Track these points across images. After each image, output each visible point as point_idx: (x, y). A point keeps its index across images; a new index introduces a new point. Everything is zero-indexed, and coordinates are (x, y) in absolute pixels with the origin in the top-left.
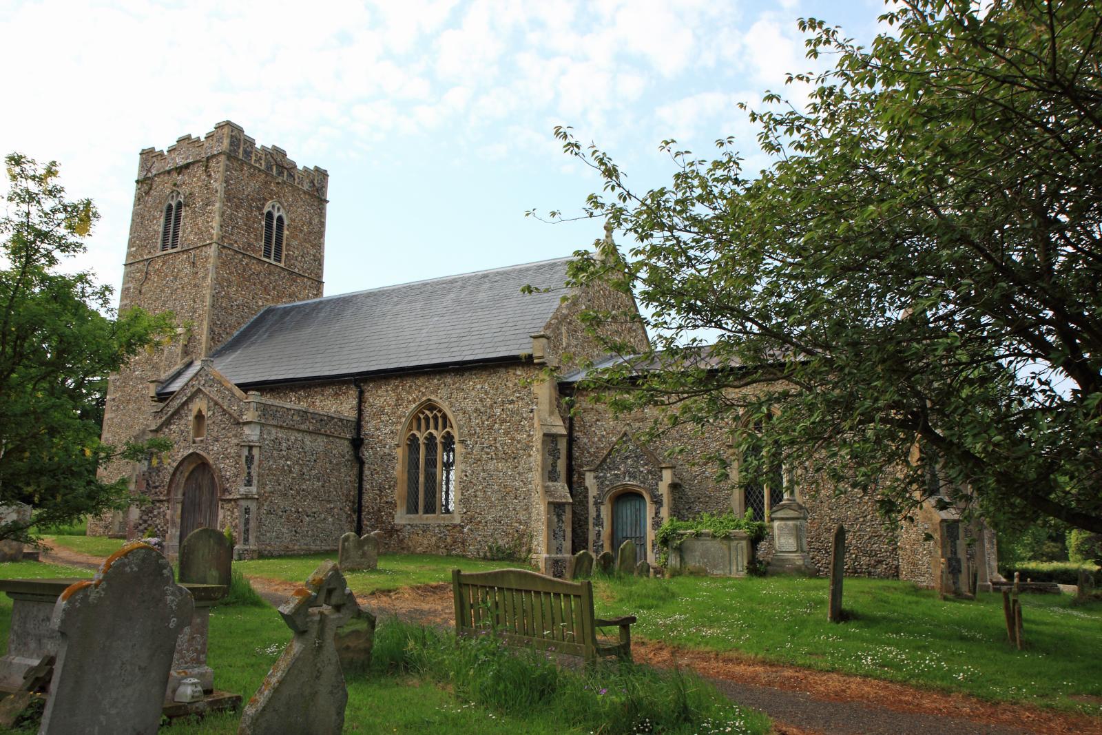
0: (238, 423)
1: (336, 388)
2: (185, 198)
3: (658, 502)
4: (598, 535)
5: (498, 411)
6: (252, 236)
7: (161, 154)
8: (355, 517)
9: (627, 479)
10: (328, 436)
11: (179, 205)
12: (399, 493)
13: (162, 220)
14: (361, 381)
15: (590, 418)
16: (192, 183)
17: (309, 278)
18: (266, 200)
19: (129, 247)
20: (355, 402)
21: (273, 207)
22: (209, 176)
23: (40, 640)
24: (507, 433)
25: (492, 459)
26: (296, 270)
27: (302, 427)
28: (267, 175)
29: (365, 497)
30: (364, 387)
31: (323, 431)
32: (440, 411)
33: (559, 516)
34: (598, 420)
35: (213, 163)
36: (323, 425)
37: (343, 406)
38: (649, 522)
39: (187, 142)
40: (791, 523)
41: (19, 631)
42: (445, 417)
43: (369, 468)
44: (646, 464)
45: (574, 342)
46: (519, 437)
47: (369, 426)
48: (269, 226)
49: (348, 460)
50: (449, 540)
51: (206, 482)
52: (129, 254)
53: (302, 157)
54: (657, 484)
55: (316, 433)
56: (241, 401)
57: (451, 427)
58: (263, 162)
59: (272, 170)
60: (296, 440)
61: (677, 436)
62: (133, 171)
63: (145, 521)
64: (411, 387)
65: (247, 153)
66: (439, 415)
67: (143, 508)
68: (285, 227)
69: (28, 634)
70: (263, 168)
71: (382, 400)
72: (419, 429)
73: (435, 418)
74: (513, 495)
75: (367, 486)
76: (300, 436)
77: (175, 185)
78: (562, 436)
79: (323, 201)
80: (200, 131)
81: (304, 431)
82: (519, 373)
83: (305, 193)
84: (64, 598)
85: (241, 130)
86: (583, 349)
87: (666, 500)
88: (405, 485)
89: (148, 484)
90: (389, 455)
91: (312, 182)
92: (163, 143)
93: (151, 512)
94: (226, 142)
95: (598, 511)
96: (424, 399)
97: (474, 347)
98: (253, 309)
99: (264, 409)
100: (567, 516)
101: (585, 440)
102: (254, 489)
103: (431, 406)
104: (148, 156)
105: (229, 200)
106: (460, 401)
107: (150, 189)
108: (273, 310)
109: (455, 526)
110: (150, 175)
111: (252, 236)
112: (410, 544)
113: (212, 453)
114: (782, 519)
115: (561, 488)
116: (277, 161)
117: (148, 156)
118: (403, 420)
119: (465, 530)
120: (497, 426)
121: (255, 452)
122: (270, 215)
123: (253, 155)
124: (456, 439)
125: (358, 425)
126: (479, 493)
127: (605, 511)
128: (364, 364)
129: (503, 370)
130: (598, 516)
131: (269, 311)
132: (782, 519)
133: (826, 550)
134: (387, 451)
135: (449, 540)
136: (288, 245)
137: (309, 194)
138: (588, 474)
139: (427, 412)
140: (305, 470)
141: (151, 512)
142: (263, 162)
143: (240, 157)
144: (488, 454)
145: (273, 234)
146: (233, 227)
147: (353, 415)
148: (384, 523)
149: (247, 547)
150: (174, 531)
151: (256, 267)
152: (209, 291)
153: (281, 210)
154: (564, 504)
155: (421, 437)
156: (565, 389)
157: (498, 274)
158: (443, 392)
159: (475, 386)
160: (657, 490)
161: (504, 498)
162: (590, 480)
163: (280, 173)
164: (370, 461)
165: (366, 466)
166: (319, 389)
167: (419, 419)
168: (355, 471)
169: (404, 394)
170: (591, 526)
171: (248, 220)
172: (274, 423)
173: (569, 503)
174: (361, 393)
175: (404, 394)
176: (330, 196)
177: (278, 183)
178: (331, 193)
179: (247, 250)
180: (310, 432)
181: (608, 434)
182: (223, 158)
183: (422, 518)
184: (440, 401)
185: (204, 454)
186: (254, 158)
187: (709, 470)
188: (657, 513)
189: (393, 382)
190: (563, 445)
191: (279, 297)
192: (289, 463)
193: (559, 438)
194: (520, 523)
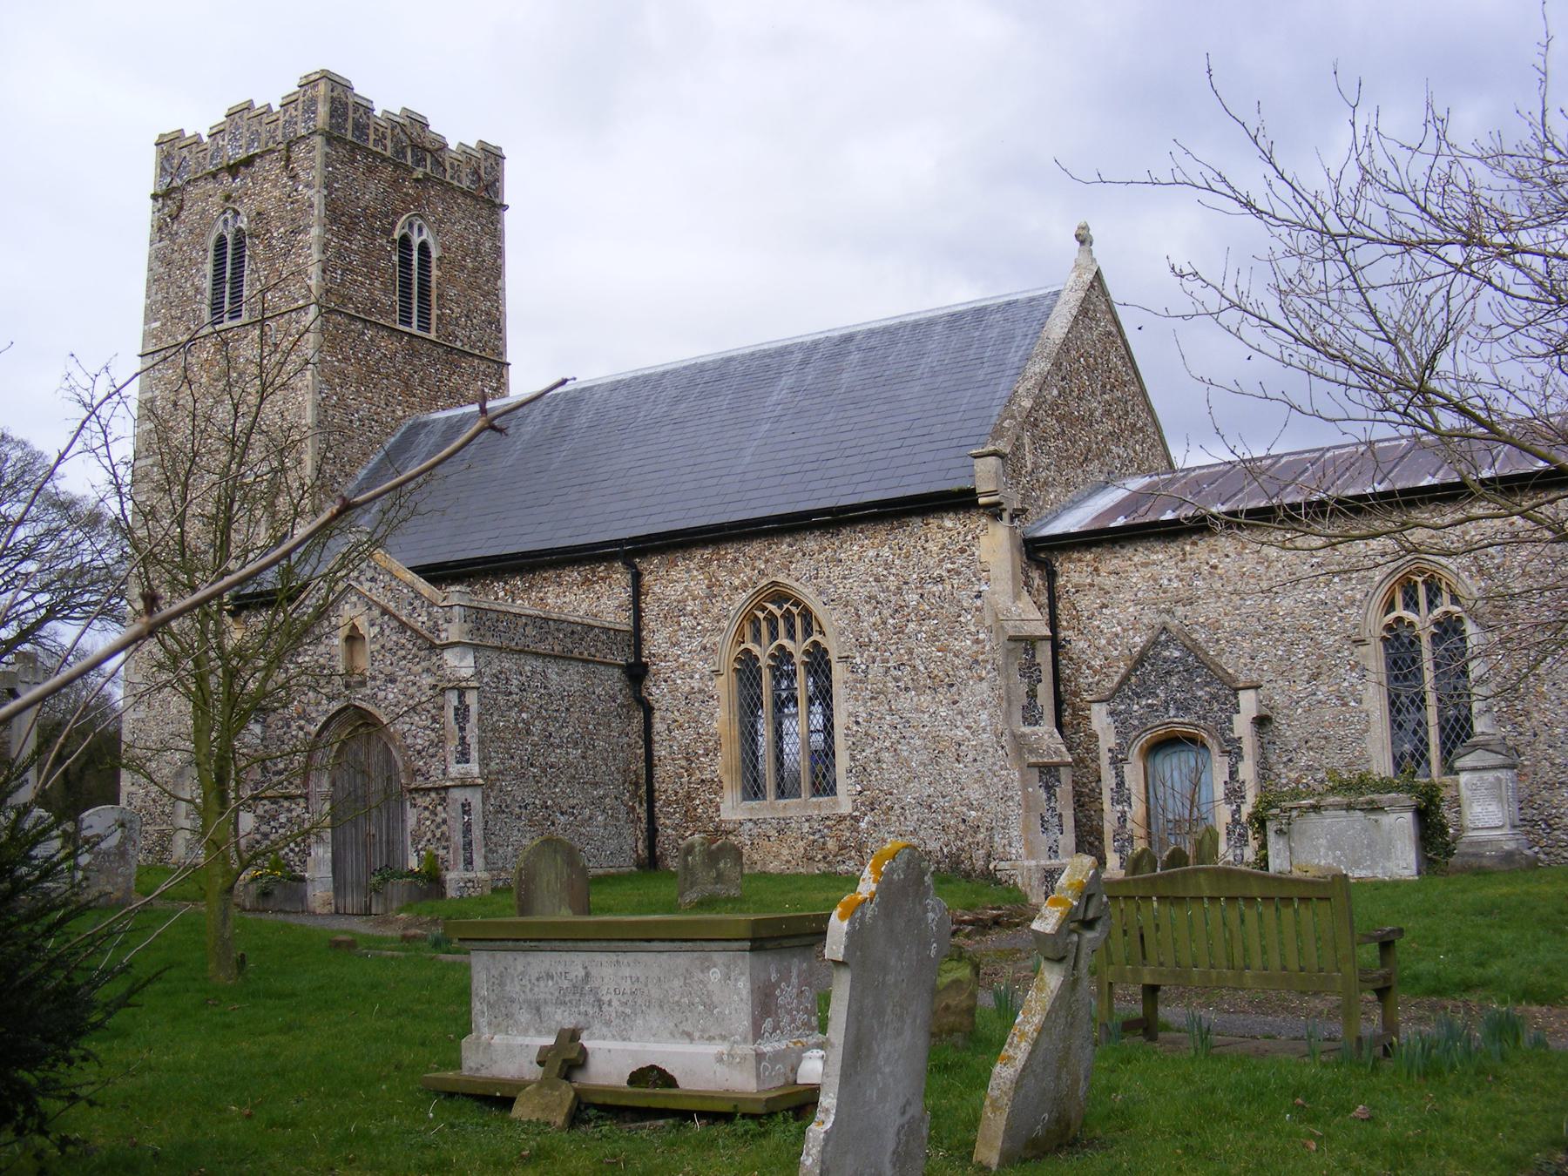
0: (432, 647)
1: (586, 570)
2: (250, 222)
3: (1233, 750)
4: (1123, 818)
5: (913, 599)
6: (377, 284)
7: (197, 140)
8: (642, 811)
9: (1172, 713)
10: (586, 661)
11: (240, 237)
12: (724, 764)
13: (208, 268)
14: (635, 552)
15: (1087, 602)
16: (265, 190)
17: (481, 358)
18: (398, 214)
19: (147, 321)
20: (625, 596)
21: (411, 225)
22: (294, 177)
23: (538, 1010)
24: (933, 638)
25: (907, 689)
26: (458, 344)
27: (542, 648)
28: (397, 166)
29: (659, 772)
30: (642, 565)
31: (576, 653)
32: (797, 603)
33: (1049, 788)
34: (1104, 606)
35: (299, 152)
36: (570, 643)
37: (597, 601)
38: (1220, 791)
39: (246, 115)
40: (1489, 776)
41: (493, 998)
42: (807, 615)
43: (663, 719)
44: (1207, 684)
45: (1045, 460)
46: (957, 645)
47: (657, 641)
48: (405, 263)
49: (622, 706)
50: (831, 844)
51: (373, 760)
52: (148, 335)
53: (457, 129)
54: (1230, 721)
55: (564, 657)
56: (433, 604)
57: (821, 632)
58: (388, 143)
59: (405, 157)
60: (533, 672)
61: (1260, 629)
62: (146, 178)
63: (266, 836)
64: (736, 560)
65: (361, 129)
66: (795, 610)
67: (260, 811)
68: (434, 264)
69: (513, 1001)
70: (388, 154)
71: (680, 587)
72: (757, 638)
73: (788, 617)
74: (951, 755)
75: (660, 751)
76: (538, 664)
77: (228, 198)
78: (1043, 638)
79: (495, 207)
80: (272, 91)
81: (545, 656)
82: (948, 524)
83: (465, 193)
84: (842, 917)
85: (347, 87)
86: (1060, 471)
87: (1248, 745)
88: (737, 747)
90: (701, 691)
91: (476, 172)
92: (200, 120)
93: (275, 818)
94: (323, 110)
95: (1119, 775)
96: (764, 582)
97: (855, 479)
98: (386, 424)
99: (478, 617)
100: (1065, 789)
101: (1082, 645)
102: (474, 768)
103: (780, 596)
104: (171, 148)
105: (333, 221)
106: (840, 582)
107: (181, 208)
108: (425, 424)
109: (841, 819)
110: (177, 182)
111: (377, 284)
112: (756, 857)
113: (385, 701)
114: (1474, 769)
115: (1045, 733)
116: (412, 144)
117: (171, 148)
118: (725, 624)
119: (863, 825)
120: (912, 626)
121: (472, 699)
122: (405, 242)
123: (371, 131)
124: (833, 656)
125: (636, 637)
126: (886, 756)
127: (1133, 774)
128: (641, 521)
129: (918, 521)
130: (1121, 784)
131: (416, 429)
132: (1474, 769)
133: (1546, 822)
134: (696, 684)
135: (831, 844)
136: (440, 297)
137: (474, 197)
138: (1095, 707)
139: (771, 607)
140: (552, 729)
141: (275, 818)
142: (388, 143)
143: (349, 137)
144: (897, 680)
145: (412, 278)
146: (344, 271)
147: (624, 621)
148: (699, 819)
149: (471, 875)
150: (321, 851)
151: (387, 345)
152: (309, 397)
153: (425, 230)
154: (1057, 766)
155: (763, 653)
156: (1041, 554)
157: (871, 333)
158: (802, 567)
159: (864, 552)
160: (1231, 730)
161: (935, 761)
162: (1099, 718)
163: (419, 161)
164: (664, 704)
165: (657, 714)
166: (551, 574)
167: (755, 621)
168: (637, 722)
169: (722, 575)
170: (1107, 806)
171: (368, 255)
172: (497, 643)
173: (1067, 765)
174: (637, 578)
175: (722, 575)
176: (510, 195)
177: (417, 180)
178: (513, 189)
179: (371, 314)
180: (556, 657)
181: (1124, 630)
182: (318, 140)
183: (770, 808)
184: (795, 584)
185: (371, 708)
186: (372, 137)
187: (1322, 688)
188: (1233, 774)
189: (698, 553)
190: (1044, 655)
191: (431, 402)
192: (524, 715)
193: (1038, 644)
194: (971, 807)
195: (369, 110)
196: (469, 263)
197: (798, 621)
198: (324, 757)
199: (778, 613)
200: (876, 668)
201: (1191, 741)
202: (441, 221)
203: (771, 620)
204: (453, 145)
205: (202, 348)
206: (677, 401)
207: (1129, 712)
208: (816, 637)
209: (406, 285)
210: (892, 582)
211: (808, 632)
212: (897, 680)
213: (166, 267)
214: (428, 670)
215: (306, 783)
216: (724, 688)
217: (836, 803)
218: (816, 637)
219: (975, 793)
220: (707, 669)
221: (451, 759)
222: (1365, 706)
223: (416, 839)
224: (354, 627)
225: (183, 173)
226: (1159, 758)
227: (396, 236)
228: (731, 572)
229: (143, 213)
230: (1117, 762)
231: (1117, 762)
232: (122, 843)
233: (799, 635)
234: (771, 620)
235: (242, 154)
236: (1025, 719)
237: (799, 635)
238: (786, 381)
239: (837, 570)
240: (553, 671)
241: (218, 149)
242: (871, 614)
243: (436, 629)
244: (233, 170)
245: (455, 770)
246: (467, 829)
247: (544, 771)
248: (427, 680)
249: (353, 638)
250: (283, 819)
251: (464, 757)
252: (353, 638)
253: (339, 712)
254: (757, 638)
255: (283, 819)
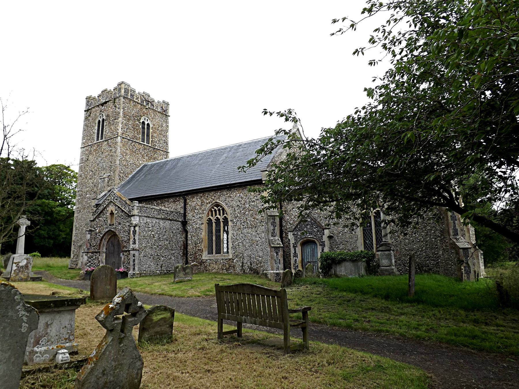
7: (94, 98)
11: (103, 120)
12: (204, 246)
13: (96, 128)
14: (185, 195)
19: (83, 140)
22: (115, 106)
26: (156, 147)
27: (158, 217)
32: (221, 207)
33: (277, 253)
35: (117, 100)
42: (223, 209)
46: (257, 217)
47: (189, 216)
48: (143, 128)
53: (157, 97)
58: (139, 99)
60: (156, 222)
62: (83, 106)
63: (90, 262)
64: (208, 196)
66: (221, 209)
67: (89, 256)
70: (139, 102)
71: (195, 203)
72: (212, 216)
73: (219, 210)
75: (189, 242)
76: (158, 221)
80: (111, 86)
89: (90, 245)
92: (95, 94)
93: (92, 257)
94: (123, 91)
95: (295, 250)
100: (281, 253)
101: (288, 218)
103: (218, 205)
104: (89, 99)
106: (231, 202)
109: (230, 259)
116: (146, 102)
117: (89, 99)
120: (247, 213)
122: (143, 123)
123: (135, 96)
124: (229, 220)
125: (185, 215)
126: (240, 244)
127: (299, 249)
130: (295, 252)
136: (152, 136)
138: (289, 233)
139: (215, 208)
141: (92, 257)
143: (129, 97)
144: (243, 226)
147: (182, 211)
148: (197, 259)
155: (213, 219)
158: (223, 198)
159: (237, 195)
162: (290, 236)
166: (166, 199)
167: (212, 211)
169: (205, 200)
170: (292, 257)
173: (281, 247)
175: (205, 200)
178: (171, 112)
190: (277, 220)
195: (134, 91)
196: (160, 129)
197: (221, 211)
198: (104, 242)
199: (217, 209)
200: (239, 223)
201: (313, 242)
202: (153, 118)
203: (215, 211)
204: (156, 101)
205: (94, 146)
206: (201, 160)
207: (297, 234)
208: (225, 215)
209: (143, 133)
210: (243, 202)
211: (223, 214)
212: (243, 226)
213: (87, 127)
214: (128, 222)
215: (99, 249)
216: (204, 227)
217: (229, 255)
218: (225, 215)
219: (261, 254)
220: (200, 222)
221: (131, 243)
222: (357, 234)
223: (124, 263)
224: (112, 211)
225: (93, 106)
226: (305, 246)
227: (141, 121)
228: (206, 199)
229: (82, 115)
230: (295, 247)
231: (295, 247)
232: (27, 264)
233: (221, 214)
234: (215, 211)
235: (104, 101)
236: (272, 236)
237: (221, 214)
238: (225, 155)
239: (231, 199)
240: (161, 222)
241: (99, 100)
242: (238, 210)
243: (130, 212)
244: (102, 105)
245: (132, 246)
246: (134, 260)
247: (158, 247)
248: (128, 224)
249: (112, 214)
250: (94, 258)
251: (134, 243)
252: (112, 214)
253: (107, 232)
254: (212, 216)
255: (94, 258)
